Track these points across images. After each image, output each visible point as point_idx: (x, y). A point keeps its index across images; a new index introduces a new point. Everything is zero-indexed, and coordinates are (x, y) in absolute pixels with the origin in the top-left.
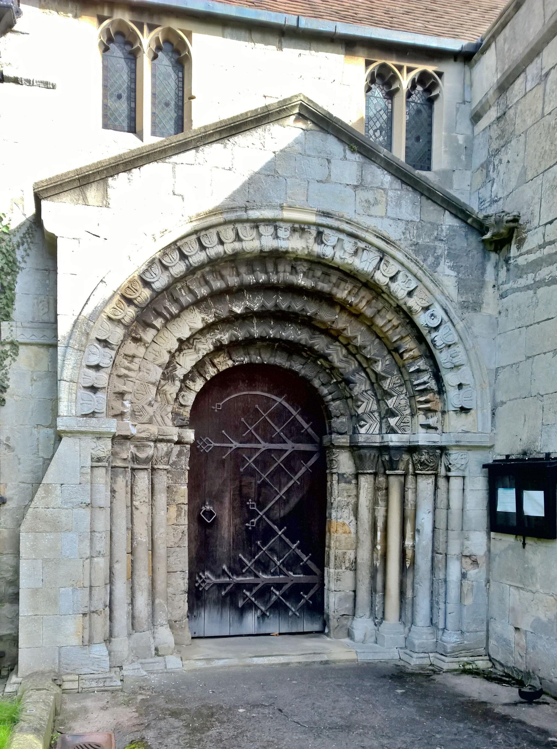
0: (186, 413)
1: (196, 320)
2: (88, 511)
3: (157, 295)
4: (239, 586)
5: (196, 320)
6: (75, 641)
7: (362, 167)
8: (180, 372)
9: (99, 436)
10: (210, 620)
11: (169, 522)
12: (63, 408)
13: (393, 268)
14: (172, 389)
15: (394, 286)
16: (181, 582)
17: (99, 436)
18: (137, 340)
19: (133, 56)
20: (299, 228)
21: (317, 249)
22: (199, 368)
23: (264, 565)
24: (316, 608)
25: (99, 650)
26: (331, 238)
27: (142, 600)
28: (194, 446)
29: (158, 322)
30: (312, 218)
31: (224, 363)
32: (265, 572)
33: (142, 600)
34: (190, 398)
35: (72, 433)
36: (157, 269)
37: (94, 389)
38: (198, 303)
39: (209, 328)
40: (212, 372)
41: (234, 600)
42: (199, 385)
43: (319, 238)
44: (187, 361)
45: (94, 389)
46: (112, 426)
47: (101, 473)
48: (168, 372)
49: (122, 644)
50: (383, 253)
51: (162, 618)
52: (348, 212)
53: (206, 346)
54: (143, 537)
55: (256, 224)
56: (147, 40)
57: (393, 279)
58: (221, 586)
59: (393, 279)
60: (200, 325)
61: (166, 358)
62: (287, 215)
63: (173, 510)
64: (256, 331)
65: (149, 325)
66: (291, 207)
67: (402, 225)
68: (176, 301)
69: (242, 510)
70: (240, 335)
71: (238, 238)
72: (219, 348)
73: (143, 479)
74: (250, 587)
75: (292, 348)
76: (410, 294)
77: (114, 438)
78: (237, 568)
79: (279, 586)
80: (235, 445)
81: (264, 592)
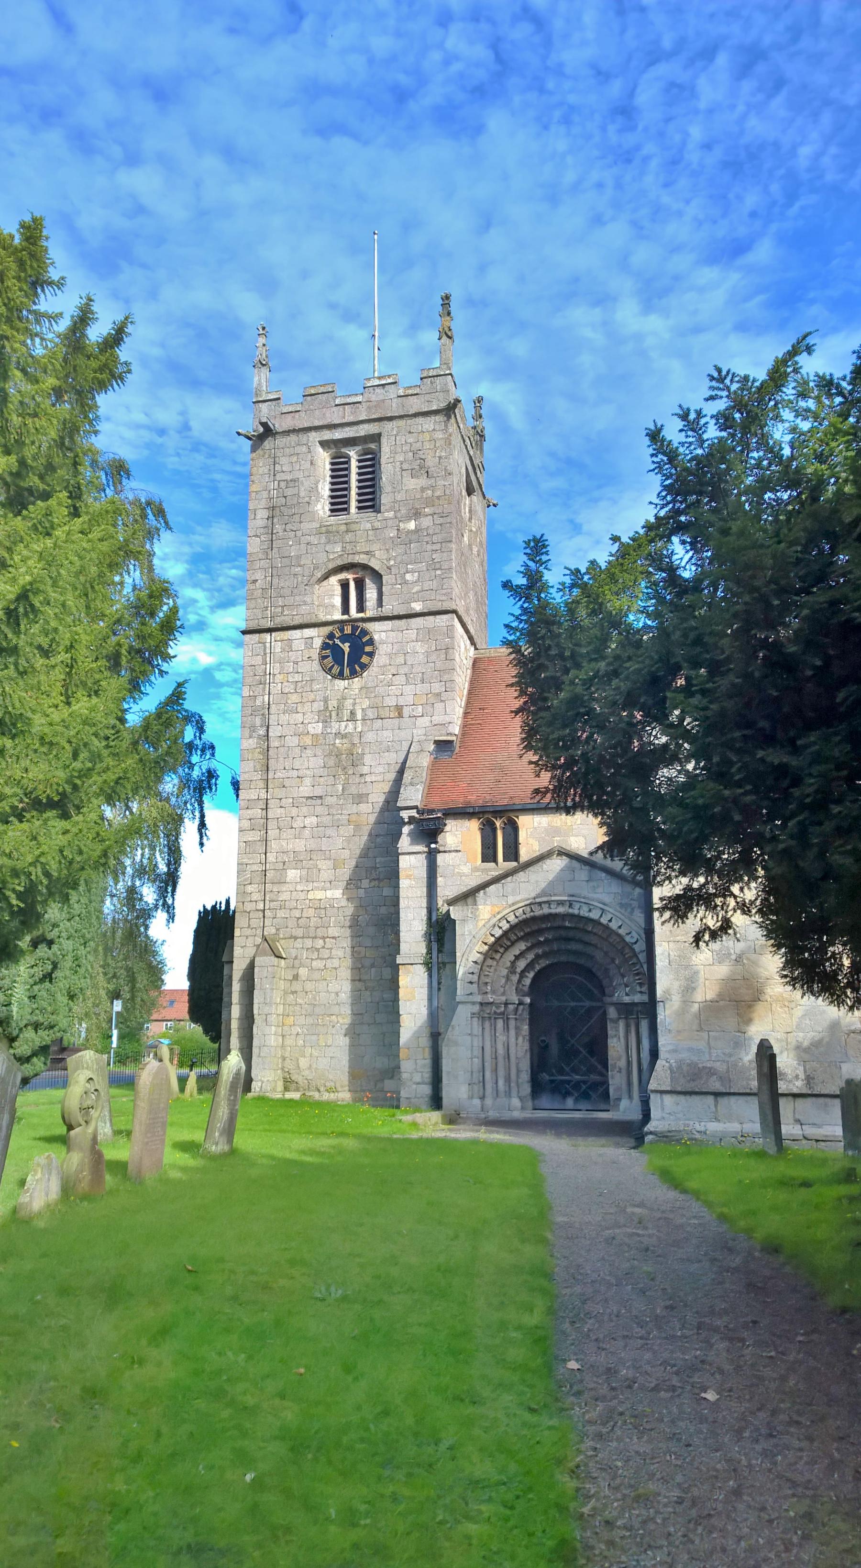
0: (526, 989)
1: (522, 946)
2: (469, 1038)
3: (498, 939)
4: (563, 1082)
5: (522, 946)
6: (465, 1096)
7: (590, 871)
8: (519, 970)
9: (474, 1003)
10: (545, 1100)
11: (517, 1043)
12: (458, 992)
13: (609, 916)
14: (515, 978)
15: (611, 924)
16: (525, 1076)
17: (474, 1003)
18: (492, 958)
19: (494, 830)
20: (560, 903)
21: (571, 911)
22: (529, 966)
23: (575, 1070)
24: (606, 1096)
25: (477, 1102)
26: (577, 906)
27: (501, 1082)
28: (531, 1005)
29: (502, 950)
30: (566, 898)
31: (543, 963)
32: (577, 1074)
33: (501, 1082)
34: (527, 982)
35: (463, 1003)
36: (497, 928)
37: (471, 983)
38: (519, 939)
39: (529, 949)
40: (538, 967)
41: (560, 1090)
42: (531, 975)
43: (571, 906)
44: (522, 964)
45: (471, 983)
46: (479, 998)
47: (475, 1019)
48: (512, 969)
49: (489, 1101)
50: (603, 910)
51: (514, 1092)
52: (585, 893)
53: (530, 956)
54: (501, 1051)
55: (540, 904)
56: (498, 823)
57: (610, 921)
58: (552, 1081)
59: (610, 921)
60: (524, 948)
61: (509, 964)
62: (553, 898)
63: (520, 1039)
64: (555, 947)
65: (497, 951)
66: (555, 895)
67: (612, 896)
68: (509, 939)
69: (562, 1040)
70: (547, 949)
71: (532, 911)
72: (538, 957)
73: (500, 1023)
74: (568, 1082)
75: (576, 953)
76: (620, 927)
77: (481, 1004)
78: (561, 1072)
79: (585, 1082)
80: (573, 1004)
81: (577, 1085)
